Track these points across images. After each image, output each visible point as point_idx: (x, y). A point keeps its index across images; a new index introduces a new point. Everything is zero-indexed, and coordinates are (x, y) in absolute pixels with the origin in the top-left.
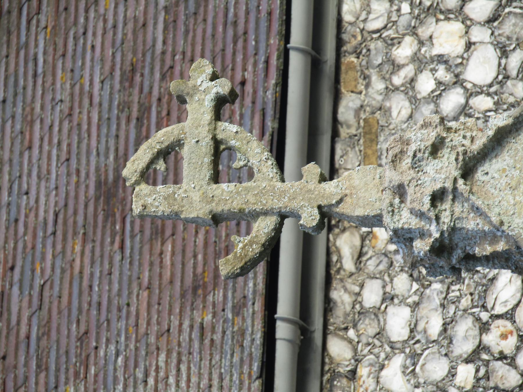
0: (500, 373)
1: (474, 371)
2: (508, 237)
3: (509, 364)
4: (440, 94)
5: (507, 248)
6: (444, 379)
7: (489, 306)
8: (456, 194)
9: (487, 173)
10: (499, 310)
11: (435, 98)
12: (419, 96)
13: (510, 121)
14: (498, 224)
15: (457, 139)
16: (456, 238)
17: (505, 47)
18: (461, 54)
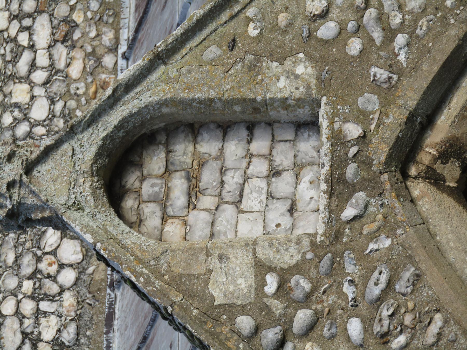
0: (48, 286)
1: (32, 284)
2: (51, 208)
3: (53, 281)
4: (16, 125)
5: (50, 215)
6: (15, 289)
7: (42, 247)
8: (22, 184)
9: (39, 172)
10: (48, 249)
11: (12, 127)
12: (3, 126)
13: (53, 142)
14: (45, 201)
15: (22, 152)
16: (21, 209)
17: (53, 99)
18: (28, 102)
